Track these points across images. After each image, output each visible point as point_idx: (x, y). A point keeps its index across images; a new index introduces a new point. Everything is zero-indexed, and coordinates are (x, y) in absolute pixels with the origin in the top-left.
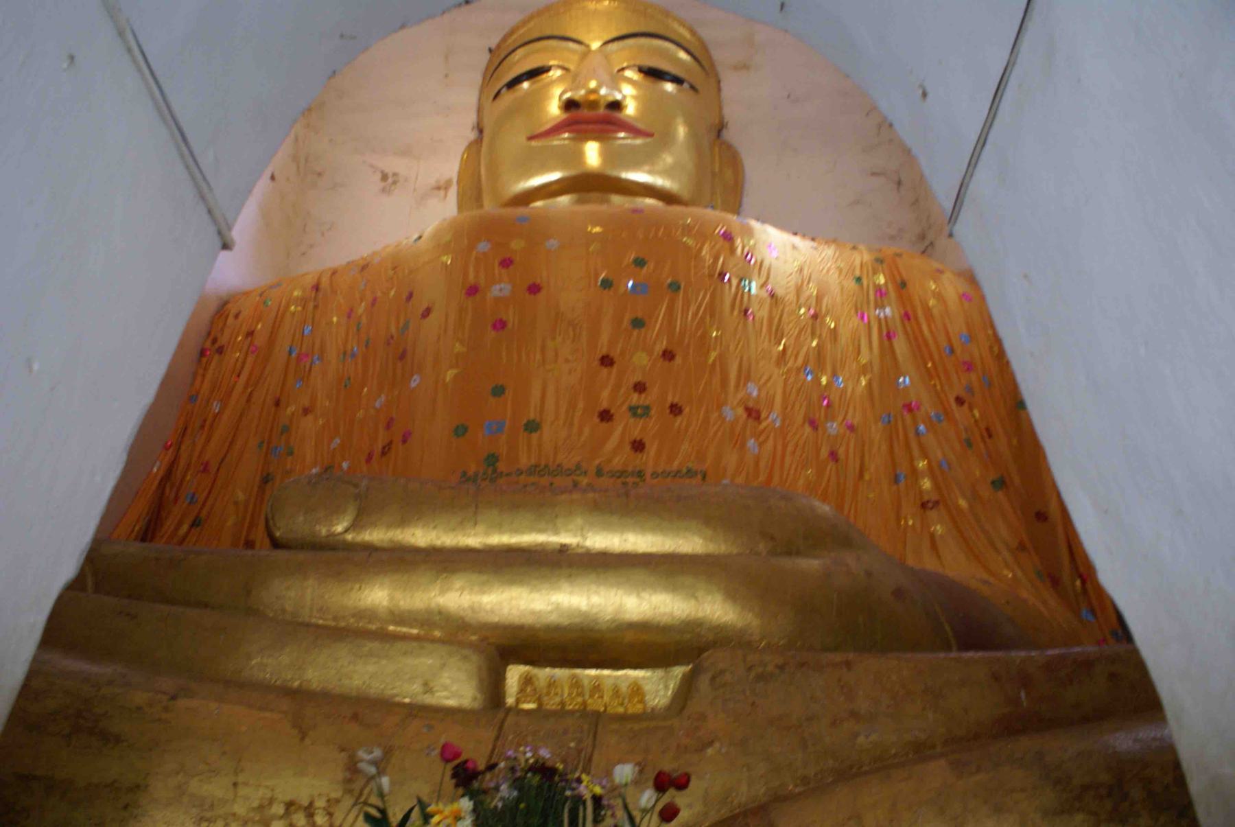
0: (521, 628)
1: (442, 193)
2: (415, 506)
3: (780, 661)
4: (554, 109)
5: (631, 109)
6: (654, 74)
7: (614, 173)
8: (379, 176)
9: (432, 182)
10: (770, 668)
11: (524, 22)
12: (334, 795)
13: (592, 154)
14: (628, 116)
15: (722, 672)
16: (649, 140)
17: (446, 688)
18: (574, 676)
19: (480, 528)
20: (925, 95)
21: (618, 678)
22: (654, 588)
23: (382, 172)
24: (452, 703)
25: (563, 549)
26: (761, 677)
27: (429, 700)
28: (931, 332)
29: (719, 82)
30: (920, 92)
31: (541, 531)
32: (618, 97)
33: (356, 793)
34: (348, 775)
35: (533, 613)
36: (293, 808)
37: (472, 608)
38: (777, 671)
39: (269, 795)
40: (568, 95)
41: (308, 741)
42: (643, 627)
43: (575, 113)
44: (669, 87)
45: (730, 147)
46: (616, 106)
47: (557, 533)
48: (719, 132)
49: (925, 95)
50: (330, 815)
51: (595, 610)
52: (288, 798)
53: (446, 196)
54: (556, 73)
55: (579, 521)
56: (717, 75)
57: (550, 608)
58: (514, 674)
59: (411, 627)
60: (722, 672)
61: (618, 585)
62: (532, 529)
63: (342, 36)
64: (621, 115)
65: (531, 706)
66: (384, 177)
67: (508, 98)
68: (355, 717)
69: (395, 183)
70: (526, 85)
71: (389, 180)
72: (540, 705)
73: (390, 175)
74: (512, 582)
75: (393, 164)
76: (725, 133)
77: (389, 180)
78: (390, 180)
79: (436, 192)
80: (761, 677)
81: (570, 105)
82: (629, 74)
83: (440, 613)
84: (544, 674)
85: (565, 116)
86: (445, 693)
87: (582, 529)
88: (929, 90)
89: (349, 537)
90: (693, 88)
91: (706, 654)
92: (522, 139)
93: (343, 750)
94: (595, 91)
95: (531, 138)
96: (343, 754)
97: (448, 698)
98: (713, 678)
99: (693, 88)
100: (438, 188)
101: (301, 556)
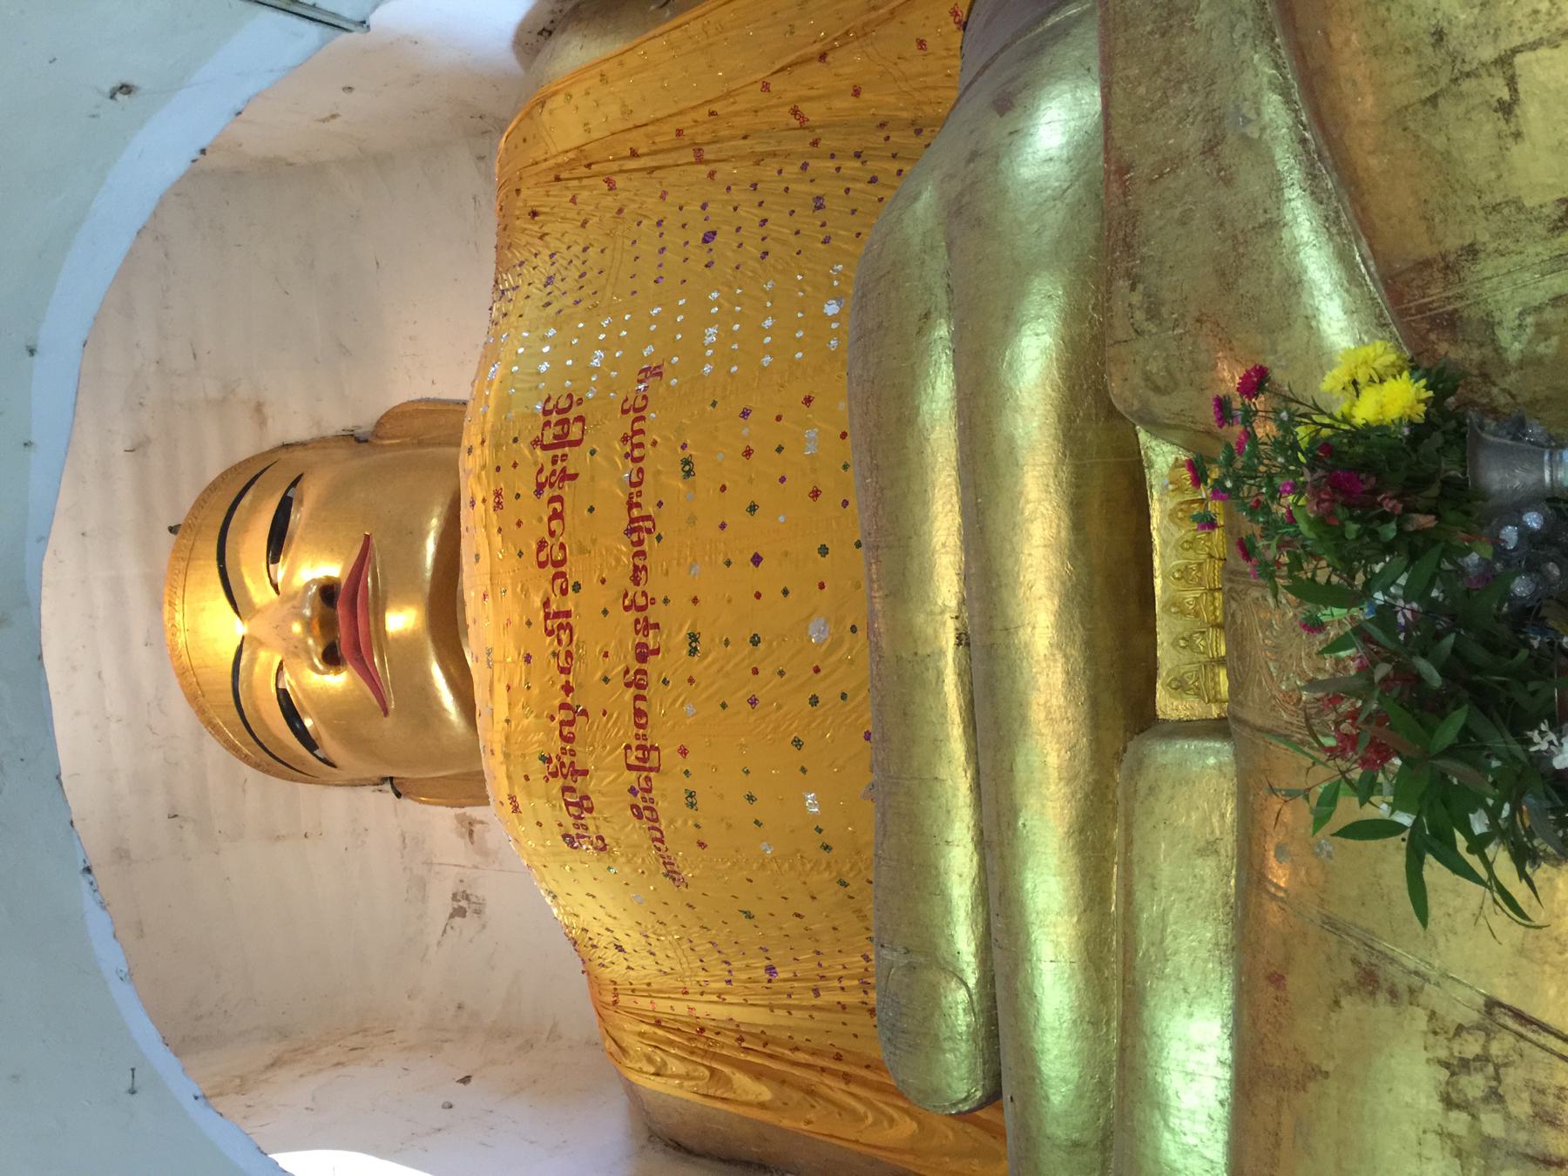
0: (1094, 703)
1: (477, 828)
2: (924, 955)
3: (1122, 284)
4: (339, 681)
5: (334, 568)
6: (277, 543)
7: (427, 588)
8: (458, 920)
9: (461, 843)
10: (1136, 298)
11: (216, 730)
12: (1422, 1023)
13: (402, 620)
14: (344, 570)
15: (1147, 377)
16: (373, 541)
17: (1206, 820)
18: (1165, 608)
19: (943, 773)
20: (126, 89)
21: (1164, 543)
22: (1016, 498)
23: (452, 916)
24: (1229, 809)
25: (963, 640)
26: (1153, 313)
27: (1228, 845)
28: (1543, 1048)
29: (286, 446)
30: (119, 96)
31: (940, 675)
32: (314, 588)
33: (1416, 981)
34: (1382, 997)
35: (1069, 683)
36: (1454, 1096)
37: (1070, 781)
38: (1140, 287)
39: (1431, 1137)
40: (320, 667)
41: (1328, 1066)
42: (1077, 507)
43: (344, 649)
44: (297, 517)
45: (379, 424)
46: (328, 592)
47: (942, 653)
48: (358, 440)
49: (126, 89)
50: (1460, 1029)
51: (1057, 585)
52: (1437, 1106)
53: (482, 822)
54: (288, 681)
55: (920, 619)
56: (273, 451)
57: (1060, 660)
58: (1169, 705)
59: (1109, 875)
60: (1147, 377)
61: (1015, 553)
62: (939, 692)
63: (133, 1092)
64: (343, 582)
65: (1223, 676)
66: (459, 912)
67: (330, 746)
68: (1277, 979)
69: (467, 898)
70: (308, 723)
71: (464, 905)
72: (1221, 662)
73: (456, 905)
74: (1023, 705)
75: (439, 904)
76: (358, 432)
77: (464, 905)
78: (463, 903)
79: (475, 836)
80: (1153, 313)
81: (332, 658)
82: (279, 580)
83: (1082, 831)
84: (1168, 656)
85: (350, 667)
86: (1215, 820)
87: (932, 613)
88: (117, 84)
89: (972, 981)
90: (294, 484)
91: (1119, 407)
92: (388, 722)
93: (1337, 1003)
94: (308, 625)
95: (386, 713)
96: (1343, 1003)
97: (1223, 816)
98: (1157, 389)
99: (294, 484)
100: (471, 833)
101: (1008, 1060)
